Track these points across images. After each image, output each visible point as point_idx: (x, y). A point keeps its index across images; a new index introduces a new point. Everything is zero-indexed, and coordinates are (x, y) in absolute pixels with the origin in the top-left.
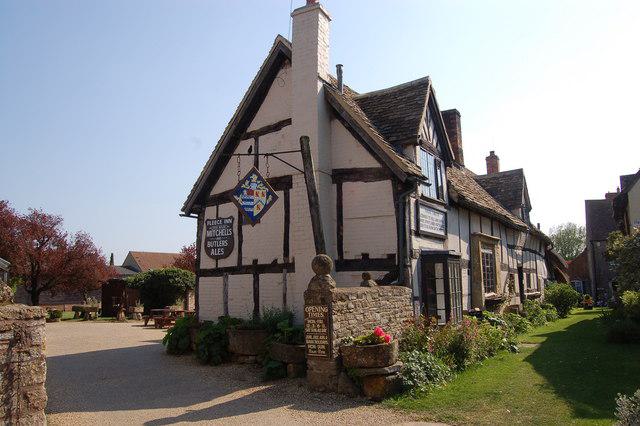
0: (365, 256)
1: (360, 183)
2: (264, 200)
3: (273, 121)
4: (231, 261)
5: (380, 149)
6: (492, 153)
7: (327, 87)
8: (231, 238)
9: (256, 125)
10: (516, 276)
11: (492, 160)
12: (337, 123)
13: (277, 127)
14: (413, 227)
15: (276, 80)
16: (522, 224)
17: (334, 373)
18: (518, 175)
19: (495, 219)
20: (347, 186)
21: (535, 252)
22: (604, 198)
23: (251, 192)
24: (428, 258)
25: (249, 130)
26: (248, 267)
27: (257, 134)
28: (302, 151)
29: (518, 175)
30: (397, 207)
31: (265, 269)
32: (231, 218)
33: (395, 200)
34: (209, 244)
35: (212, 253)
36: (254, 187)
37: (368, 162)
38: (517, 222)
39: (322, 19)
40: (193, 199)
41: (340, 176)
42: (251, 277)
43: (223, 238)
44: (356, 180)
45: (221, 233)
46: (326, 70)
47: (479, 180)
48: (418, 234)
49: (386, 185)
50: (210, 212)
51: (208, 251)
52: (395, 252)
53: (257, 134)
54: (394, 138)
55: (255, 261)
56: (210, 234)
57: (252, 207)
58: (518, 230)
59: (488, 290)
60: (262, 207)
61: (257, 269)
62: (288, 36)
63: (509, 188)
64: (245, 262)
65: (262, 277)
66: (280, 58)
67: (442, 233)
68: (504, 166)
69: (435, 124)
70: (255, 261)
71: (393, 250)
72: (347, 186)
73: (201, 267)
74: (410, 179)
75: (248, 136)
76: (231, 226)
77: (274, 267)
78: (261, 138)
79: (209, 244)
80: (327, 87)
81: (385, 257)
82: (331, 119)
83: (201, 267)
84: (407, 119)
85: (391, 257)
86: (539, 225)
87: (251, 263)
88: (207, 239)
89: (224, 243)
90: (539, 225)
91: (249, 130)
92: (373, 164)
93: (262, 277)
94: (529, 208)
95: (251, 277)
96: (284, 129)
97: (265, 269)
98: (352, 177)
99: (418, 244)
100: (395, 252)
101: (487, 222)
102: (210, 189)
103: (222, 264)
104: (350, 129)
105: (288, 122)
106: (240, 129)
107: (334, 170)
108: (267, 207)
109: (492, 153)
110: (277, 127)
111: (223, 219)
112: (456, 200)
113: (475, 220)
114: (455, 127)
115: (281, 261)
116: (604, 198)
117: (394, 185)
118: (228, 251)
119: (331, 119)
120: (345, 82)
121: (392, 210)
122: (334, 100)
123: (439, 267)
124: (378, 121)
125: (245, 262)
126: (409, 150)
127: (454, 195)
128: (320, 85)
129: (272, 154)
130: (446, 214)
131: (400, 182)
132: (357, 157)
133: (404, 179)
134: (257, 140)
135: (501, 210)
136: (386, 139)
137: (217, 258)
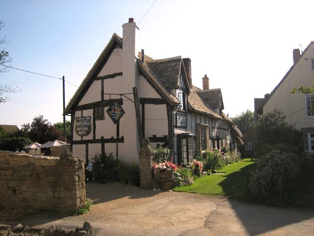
2: (120, 113)
3: (111, 73)
4: (90, 137)
5: (161, 90)
6: (206, 76)
7: (138, 60)
8: (89, 127)
9: (102, 74)
10: (216, 142)
11: (206, 80)
13: (113, 76)
14: (175, 124)
15: (112, 54)
16: (220, 117)
17: (151, 181)
18: (218, 92)
19: (207, 116)
20: (147, 106)
21: (225, 129)
22: (264, 97)
23: (115, 110)
24: (180, 136)
25: (98, 76)
26: (99, 140)
27: (102, 79)
28: (134, 93)
29: (218, 92)
30: (168, 116)
31: (108, 141)
32: (90, 117)
33: (168, 113)
34: (78, 129)
35: (80, 133)
36: (116, 108)
37: (156, 96)
38: (217, 116)
39: (136, 29)
40: (70, 107)
41: (145, 101)
42: (100, 145)
43: (85, 126)
45: (85, 124)
46: (137, 51)
47: (200, 94)
49: (164, 106)
50: (78, 114)
51: (77, 132)
52: (167, 134)
53: (102, 79)
54: (167, 86)
55: (102, 138)
56: (78, 124)
57: (115, 116)
58: (217, 119)
59: (203, 149)
60: (119, 116)
61: (103, 141)
62: (120, 35)
63: (213, 98)
64: (97, 138)
65: (106, 144)
66: (115, 44)
68: (212, 86)
69: (183, 76)
70: (102, 138)
71: (167, 134)
73: (74, 140)
75: (99, 79)
76: (90, 120)
77: (111, 140)
78: (105, 80)
79: (78, 129)
80: (138, 60)
81: (163, 137)
82: (139, 75)
83: (74, 140)
84: (172, 76)
85: (166, 136)
86: (228, 115)
87: (100, 138)
88: (77, 126)
89: (86, 129)
90: (228, 115)
91: (98, 76)
92: (158, 97)
93: (106, 144)
94: (222, 108)
95: (100, 145)
96: (116, 77)
97: (108, 141)
99: (177, 131)
100: (167, 134)
101: (203, 118)
102: (78, 103)
103: (85, 138)
104: (148, 80)
105: (121, 74)
106: (94, 76)
108: (121, 116)
109: (206, 76)
110: (113, 76)
111: (85, 117)
113: (198, 116)
114: (188, 67)
115: (115, 137)
116: (264, 97)
117: (167, 106)
118: (88, 133)
119: (139, 75)
121: (166, 117)
122: (141, 68)
123: (184, 141)
124: (160, 75)
125: (97, 138)
126: (173, 91)
128: (136, 60)
129: (122, 95)
131: (170, 105)
132: (150, 92)
133: (172, 105)
134: (103, 81)
135: (209, 111)
136: (164, 86)
137: (82, 136)
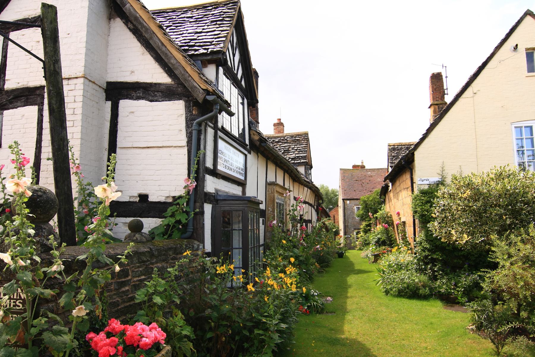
0: (144, 197)
1: (143, 103)
5: (148, 29)
12: (118, 24)
20: (125, 105)
44: (138, 98)
48: (215, 173)
55: (44, 77)
67: (243, 178)
72: (125, 105)
74: (210, 98)
81: (170, 200)
82: (110, 18)
98: (140, 93)
105: (517, 45)
107: (109, 84)
112: (258, 143)
113: (272, 168)
117: (188, 108)
119: (110, 18)
120: (81, 74)
121: (183, 140)
127: (256, 138)
130: (246, 155)
